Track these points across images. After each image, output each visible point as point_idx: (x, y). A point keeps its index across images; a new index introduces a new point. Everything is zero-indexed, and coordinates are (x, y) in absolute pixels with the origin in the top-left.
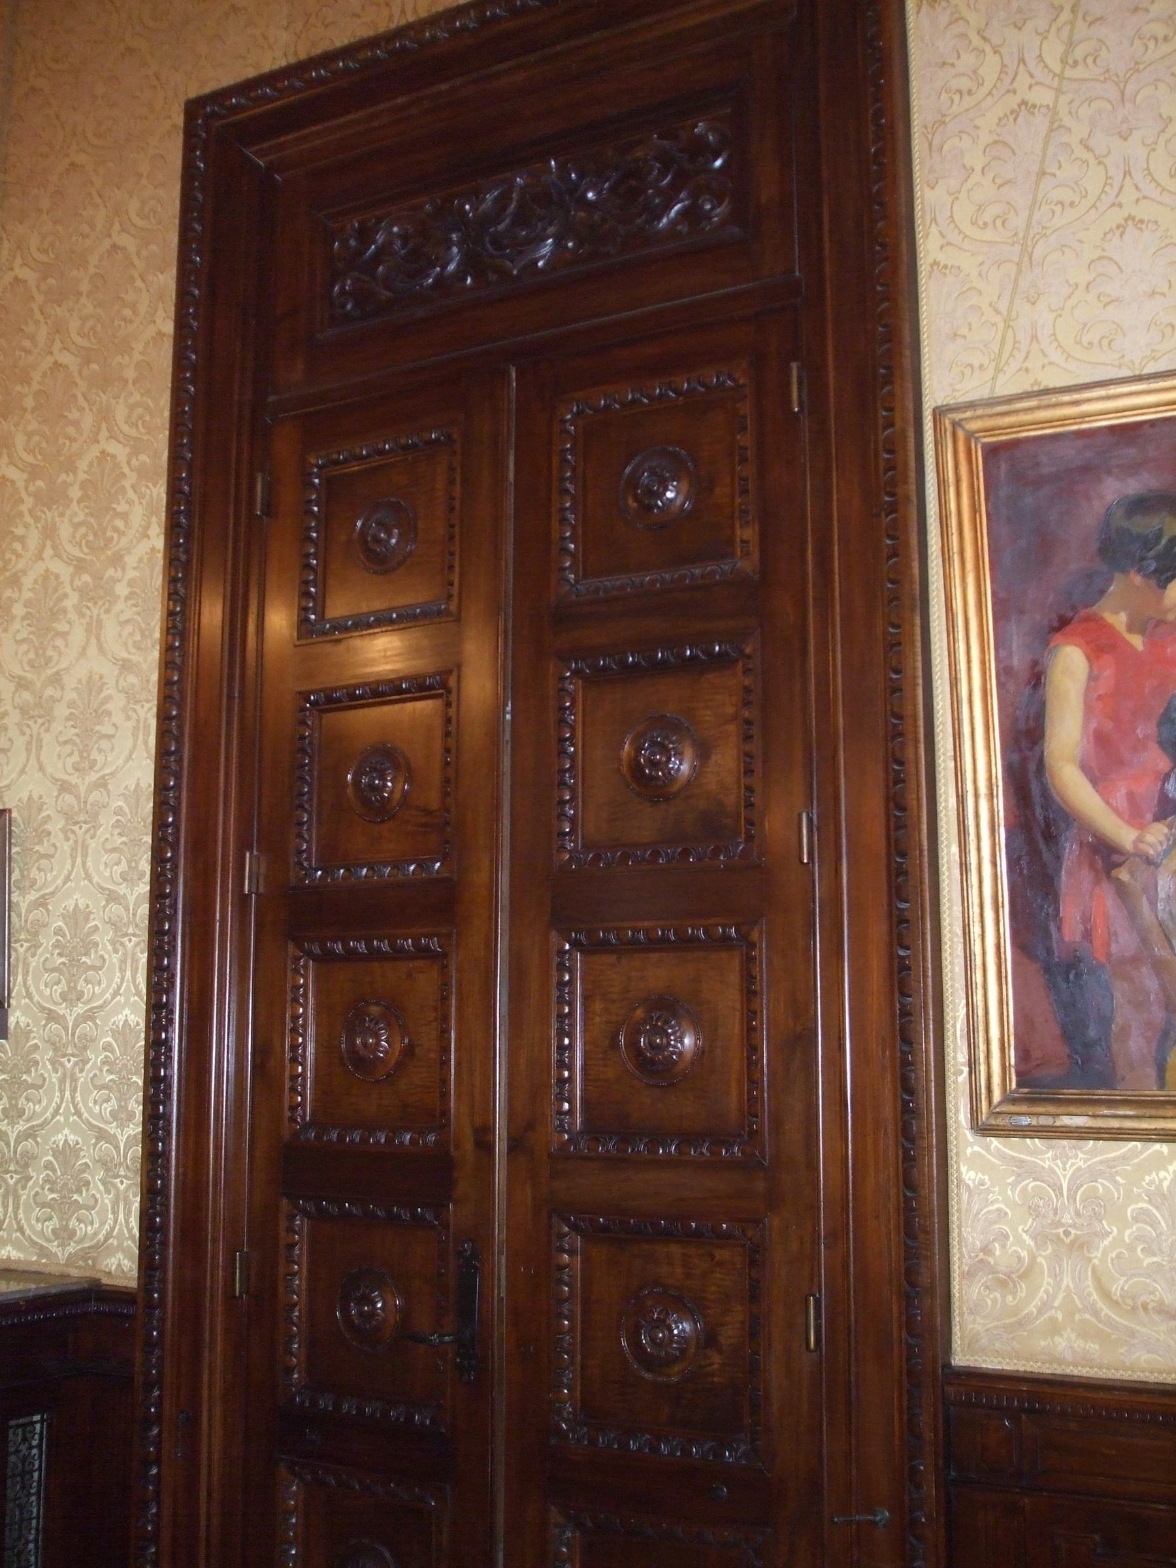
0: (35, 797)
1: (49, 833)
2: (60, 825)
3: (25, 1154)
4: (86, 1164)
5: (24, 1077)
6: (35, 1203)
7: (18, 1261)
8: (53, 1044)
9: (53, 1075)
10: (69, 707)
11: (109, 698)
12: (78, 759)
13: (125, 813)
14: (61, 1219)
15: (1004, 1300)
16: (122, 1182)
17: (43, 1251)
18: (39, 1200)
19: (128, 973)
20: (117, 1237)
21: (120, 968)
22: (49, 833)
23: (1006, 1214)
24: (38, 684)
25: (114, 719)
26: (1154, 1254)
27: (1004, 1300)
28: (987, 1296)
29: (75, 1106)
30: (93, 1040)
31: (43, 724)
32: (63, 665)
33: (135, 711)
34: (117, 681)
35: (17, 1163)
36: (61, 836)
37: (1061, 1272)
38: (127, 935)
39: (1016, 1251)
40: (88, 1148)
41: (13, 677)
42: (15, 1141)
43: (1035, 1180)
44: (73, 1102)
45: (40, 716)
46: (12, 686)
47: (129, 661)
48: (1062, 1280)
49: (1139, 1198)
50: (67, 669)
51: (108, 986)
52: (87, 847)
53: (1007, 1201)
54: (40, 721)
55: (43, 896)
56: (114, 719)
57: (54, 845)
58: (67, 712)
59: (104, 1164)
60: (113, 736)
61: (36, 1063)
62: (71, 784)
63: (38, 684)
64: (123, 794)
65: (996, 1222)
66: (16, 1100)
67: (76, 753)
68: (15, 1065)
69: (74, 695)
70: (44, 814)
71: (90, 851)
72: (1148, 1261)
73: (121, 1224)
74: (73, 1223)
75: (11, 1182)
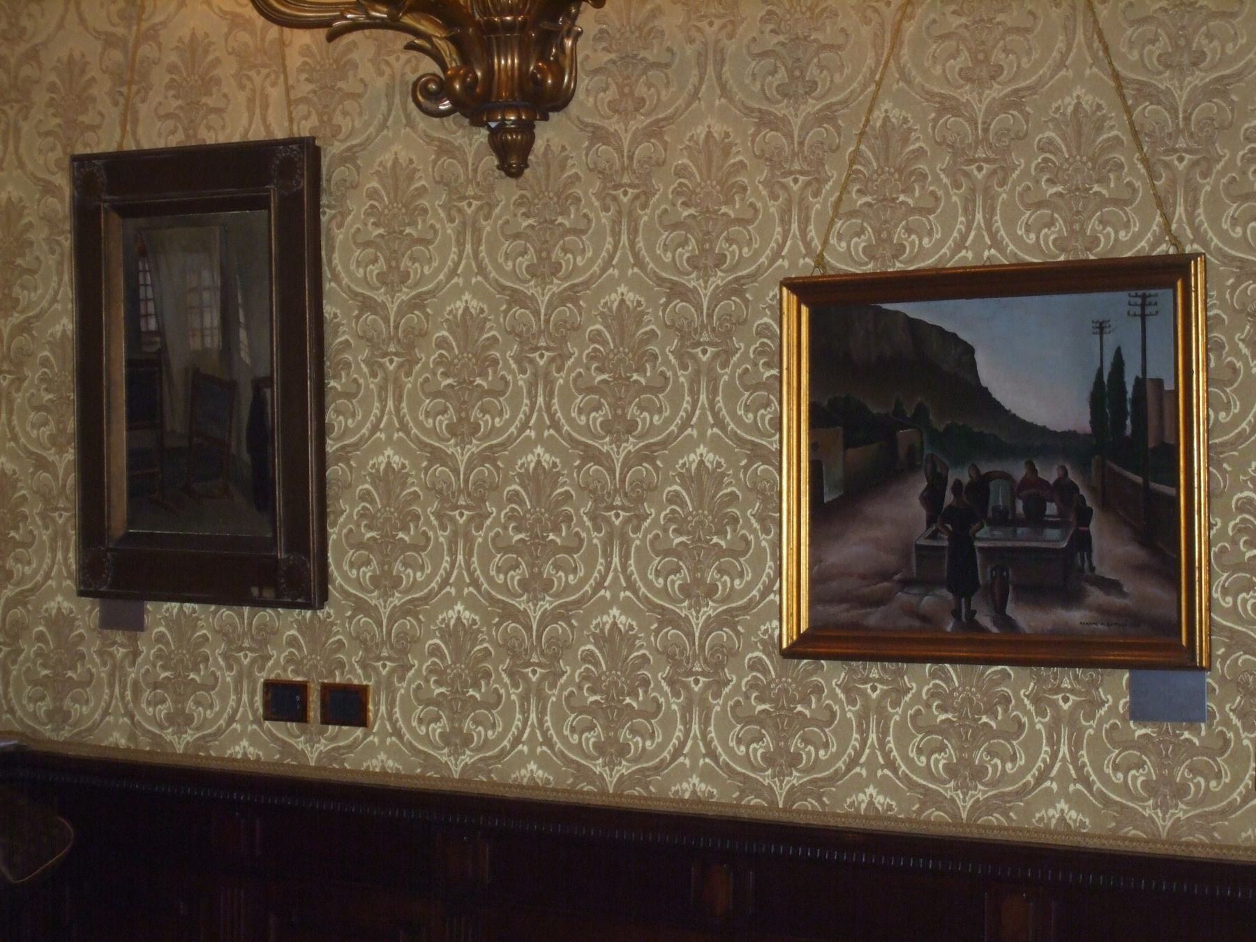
0: (556, 149)
1: (31, 243)
2: (43, 235)
3: (403, 635)
4: (339, 641)
5: (552, 536)
6: (417, 699)
7: (397, 775)
8: (594, 492)
9: (440, 533)
10: (170, 72)
11: (217, 62)
12: (317, 124)
13: (692, 175)
14: (175, 702)
15: (1003, 767)
16: (534, 672)
17: (749, 785)
18: (921, 723)
19: (390, 403)
20: (867, 764)
21: (380, 396)
22: (31, 243)
23: (1214, 690)
24: (13, 61)
25: (361, 74)
26: (946, 712)
27: (1003, 767)
28: (1191, 780)
29: (471, 574)
30: (652, 488)
31: (268, 76)
32: (39, 39)
33: (388, 63)
34: (226, 40)
35: (392, 647)
36: (46, 247)
37: (868, 726)
38: (699, 344)
39: (1222, 732)
40: (648, 637)
41: (100, 33)
42: (539, 625)
43: (1245, 653)
44: (468, 569)
45: (264, 66)
46: (98, 46)
47: (113, 34)
48: (1058, 749)
49: (754, 648)
50: (164, 24)
51: (513, 418)
52: (808, 208)
53: (649, 647)
54: (265, 71)
55: (419, 295)
56: (361, 74)
57: (37, 258)
58: (167, 78)
59: (671, 657)
60: (360, 96)
61: (25, 517)
62: (607, 131)
63: (13, 61)
64: (378, 172)
65: (998, 684)
66: (390, 565)
67: (180, 130)
68: (387, 520)
69: (53, 77)
70: (25, 221)
71: (337, 245)
72: (943, 717)
73: (695, 737)
74: (468, 725)
75: (246, 662)
